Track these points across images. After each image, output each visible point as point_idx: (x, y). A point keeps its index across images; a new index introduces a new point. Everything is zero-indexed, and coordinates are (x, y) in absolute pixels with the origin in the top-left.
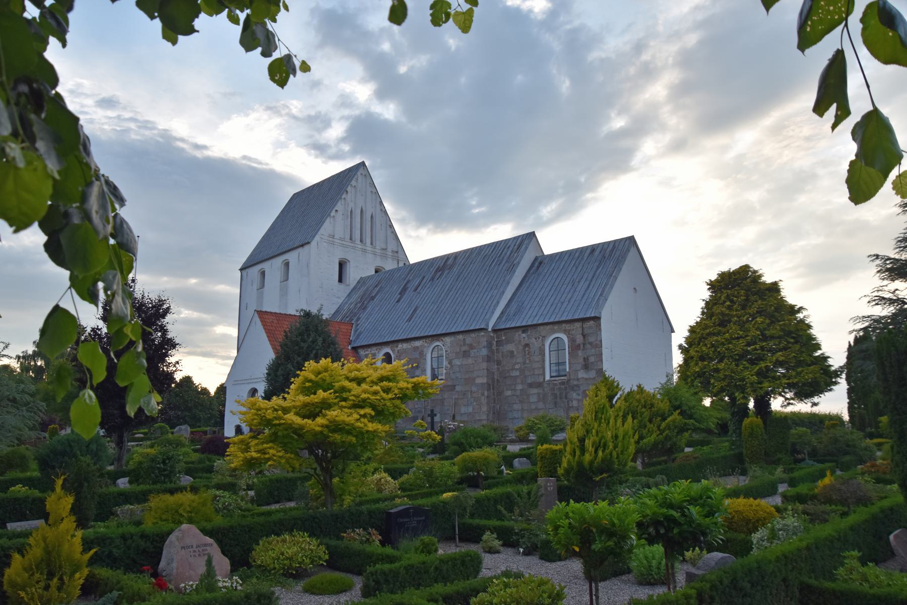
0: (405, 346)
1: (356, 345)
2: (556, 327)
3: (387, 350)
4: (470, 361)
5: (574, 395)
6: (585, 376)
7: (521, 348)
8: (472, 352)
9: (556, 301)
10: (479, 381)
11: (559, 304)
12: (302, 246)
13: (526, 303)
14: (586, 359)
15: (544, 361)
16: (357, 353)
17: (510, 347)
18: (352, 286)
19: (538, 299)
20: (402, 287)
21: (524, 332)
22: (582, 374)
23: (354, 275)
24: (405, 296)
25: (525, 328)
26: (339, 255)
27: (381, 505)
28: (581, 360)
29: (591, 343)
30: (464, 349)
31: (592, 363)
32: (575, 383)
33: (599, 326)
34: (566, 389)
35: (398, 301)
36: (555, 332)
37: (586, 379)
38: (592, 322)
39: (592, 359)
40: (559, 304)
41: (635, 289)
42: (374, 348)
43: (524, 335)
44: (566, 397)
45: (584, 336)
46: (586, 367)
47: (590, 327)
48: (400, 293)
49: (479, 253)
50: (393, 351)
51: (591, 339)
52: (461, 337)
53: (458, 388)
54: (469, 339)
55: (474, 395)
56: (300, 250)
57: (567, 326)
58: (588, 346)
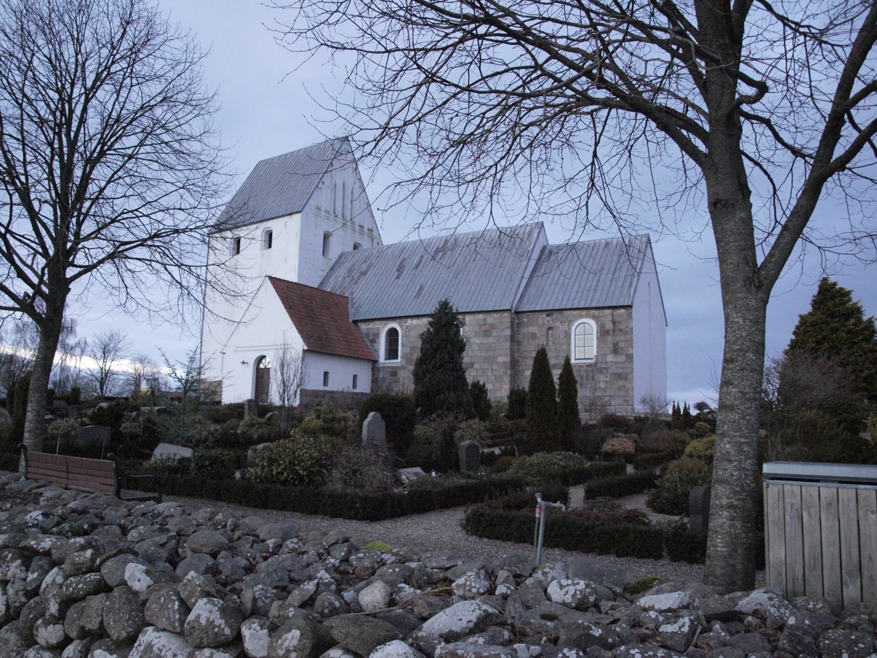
0: (415, 321)
1: (357, 318)
2: (584, 312)
3: (394, 325)
4: (491, 340)
5: (602, 378)
6: (614, 360)
7: (545, 330)
8: (494, 333)
9: (581, 289)
10: (501, 359)
11: (585, 292)
12: (290, 214)
13: (546, 289)
14: (616, 344)
15: (569, 344)
16: (357, 326)
17: (533, 329)
18: (334, 261)
19: (558, 287)
20: (398, 264)
21: (548, 315)
22: (610, 358)
23: (336, 248)
24: (404, 273)
25: (550, 312)
26: (326, 226)
27: (795, 192)
28: (611, 345)
29: (621, 330)
30: (484, 328)
31: (622, 348)
32: (603, 366)
33: (630, 316)
34: (593, 371)
35: (397, 278)
36: (582, 317)
37: (615, 363)
38: (622, 311)
39: (622, 345)
40: (585, 292)
41: (243, 363)
42: (378, 323)
43: (548, 318)
44: (593, 379)
45: (614, 323)
46: (616, 351)
47: (621, 315)
48: (398, 270)
49: (266, 164)
50: (401, 326)
51: (623, 326)
52: (481, 316)
53: (476, 366)
54: (491, 319)
55: (496, 373)
56: (287, 218)
57: (596, 313)
58: (617, 332)
